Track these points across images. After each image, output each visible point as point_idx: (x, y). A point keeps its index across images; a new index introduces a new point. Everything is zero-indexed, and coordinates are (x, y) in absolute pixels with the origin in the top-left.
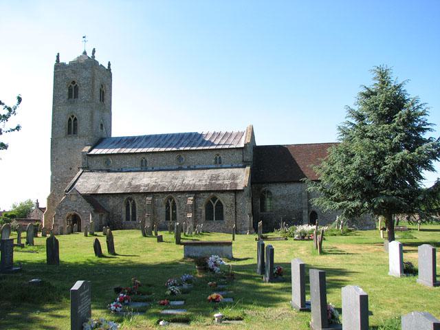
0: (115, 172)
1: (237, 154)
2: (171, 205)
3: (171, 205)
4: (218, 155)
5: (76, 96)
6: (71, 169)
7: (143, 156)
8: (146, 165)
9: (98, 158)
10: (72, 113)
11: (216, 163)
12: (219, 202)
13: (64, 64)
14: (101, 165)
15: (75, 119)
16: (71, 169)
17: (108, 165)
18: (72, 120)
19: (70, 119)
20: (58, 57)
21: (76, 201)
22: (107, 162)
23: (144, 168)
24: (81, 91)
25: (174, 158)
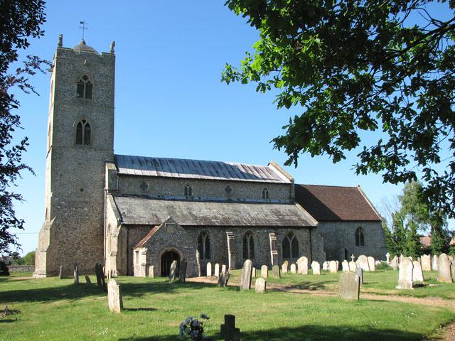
0: (156, 199)
1: (283, 189)
2: (248, 241)
3: (248, 241)
4: (265, 189)
5: (89, 95)
6: (82, 190)
7: (187, 182)
8: (190, 194)
9: (131, 180)
10: (84, 116)
11: (264, 197)
12: (295, 239)
13: (71, 52)
14: (138, 191)
15: (88, 125)
16: (82, 190)
17: (144, 190)
18: (84, 125)
19: (79, 125)
20: (61, 39)
21: (174, 234)
22: (144, 186)
23: (189, 196)
24: (345, 158)
25: (222, 188)
